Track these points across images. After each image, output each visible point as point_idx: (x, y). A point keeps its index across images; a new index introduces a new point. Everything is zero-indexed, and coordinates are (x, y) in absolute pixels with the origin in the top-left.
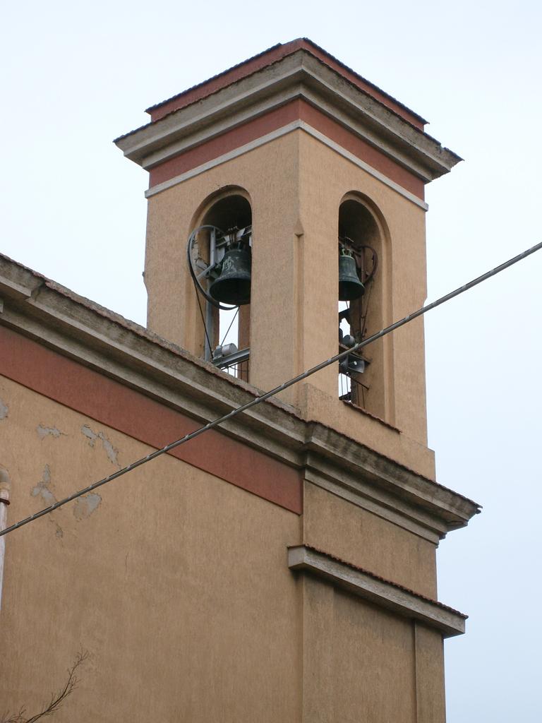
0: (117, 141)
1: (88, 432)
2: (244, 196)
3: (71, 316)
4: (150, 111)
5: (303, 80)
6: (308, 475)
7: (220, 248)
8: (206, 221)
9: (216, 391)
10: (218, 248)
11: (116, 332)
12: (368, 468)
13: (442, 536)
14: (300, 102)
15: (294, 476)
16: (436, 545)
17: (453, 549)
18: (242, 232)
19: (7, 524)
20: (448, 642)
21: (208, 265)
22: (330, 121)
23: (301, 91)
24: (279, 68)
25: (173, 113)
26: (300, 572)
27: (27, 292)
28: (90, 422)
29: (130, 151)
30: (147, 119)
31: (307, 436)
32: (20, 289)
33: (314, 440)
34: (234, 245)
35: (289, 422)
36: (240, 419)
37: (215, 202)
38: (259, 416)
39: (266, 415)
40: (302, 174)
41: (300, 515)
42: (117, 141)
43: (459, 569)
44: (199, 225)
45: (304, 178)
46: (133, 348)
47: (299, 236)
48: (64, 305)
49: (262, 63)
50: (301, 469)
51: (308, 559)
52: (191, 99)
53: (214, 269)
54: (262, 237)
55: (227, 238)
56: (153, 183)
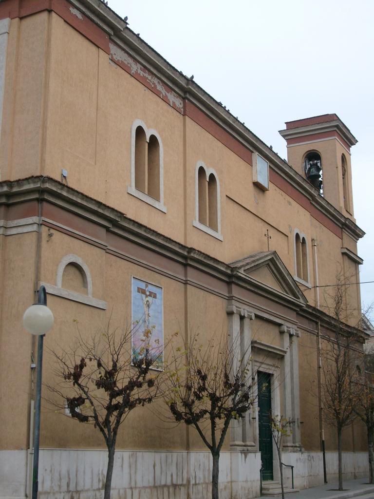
0: (279, 131)
5: (337, 126)
6: (343, 230)
11: (333, 209)
12: (353, 228)
13: (358, 240)
16: (357, 242)
17: (361, 242)
18: (315, 161)
20: (359, 265)
22: (78, 33)
23: (336, 129)
24: (331, 123)
26: (343, 254)
31: (345, 221)
33: (347, 222)
35: (325, 202)
36: (322, 206)
42: (279, 131)
43: (363, 247)
45: (329, 147)
50: (342, 228)
51: (346, 251)
55: (311, 162)
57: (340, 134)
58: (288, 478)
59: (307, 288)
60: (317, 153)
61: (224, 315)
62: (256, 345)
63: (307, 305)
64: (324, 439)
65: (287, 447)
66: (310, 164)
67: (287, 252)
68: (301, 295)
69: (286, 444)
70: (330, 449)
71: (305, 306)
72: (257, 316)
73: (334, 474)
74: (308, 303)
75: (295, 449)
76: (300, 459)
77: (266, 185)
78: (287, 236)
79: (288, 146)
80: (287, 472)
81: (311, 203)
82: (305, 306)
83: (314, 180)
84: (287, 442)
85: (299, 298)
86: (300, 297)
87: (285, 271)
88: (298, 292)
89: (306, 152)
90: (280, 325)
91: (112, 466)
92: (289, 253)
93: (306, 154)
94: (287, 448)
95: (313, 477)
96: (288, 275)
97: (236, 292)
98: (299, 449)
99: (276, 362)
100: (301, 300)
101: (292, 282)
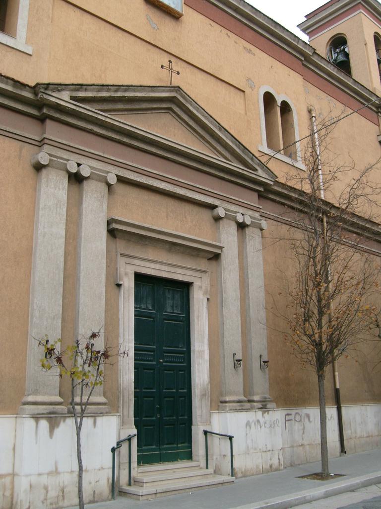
0: (298, 26)
1: (327, 98)
2: (343, 36)
3: (321, 62)
4: (306, 16)
7: (335, 53)
8: (330, 45)
9: (357, 87)
10: (335, 53)
14: (360, 4)
15: (375, 115)
18: (342, 47)
19: (300, 136)
21: (332, 59)
25: (316, 14)
27: (311, 54)
28: (328, 96)
29: (302, 28)
30: (305, 19)
32: (309, 52)
34: (340, 52)
37: (332, 40)
38: (137, 230)
39: (369, 95)
40: (364, 26)
41: (379, 126)
44: (328, 47)
46: (337, 73)
47: (365, 44)
48: (319, 59)
49: (324, 8)
50: (377, 113)
52: (324, 8)
53: (334, 60)
54: (350, 48)
55: (338, 50)
56: (310, 38)
57: (369, 9)
58: (224, 456)
59: (263, 154)
60: (344, 37)
61: (32, 171)
62: (114, 226)
63: (277, 181)
64: (338, 387)
65: (226, 402)
66: (337, 53)
67: (243, 112)
68: (258, 165)
69: (223, 399)
70: (356, 400)
71: (272, 183)
72: (121, 180)
73: (367, 437)
74: (277, 179)
75: (245, 403)
76: (258, 421)
77: (179, 9)
78: (244, 92)
79: (310, 40)
80: (219, 447)
81: (303, 64)
82: (272, 183)
83: (345, 66)
84: (253, 395)
85: (256, 170)
86: (258, 168)
87: (211, 122)
88: (252, 159)
89: (329, 42)
90: (213, 207)
91: (80, 439)
92: (246, 114)
93: (331, 41)
94: (224, 404)
95: (307, 447)
96: (220, 130)
97: (53, 131)
98: (259, 405)
99: (203, 264)
100: (260, 172)
101: (232, 142)
